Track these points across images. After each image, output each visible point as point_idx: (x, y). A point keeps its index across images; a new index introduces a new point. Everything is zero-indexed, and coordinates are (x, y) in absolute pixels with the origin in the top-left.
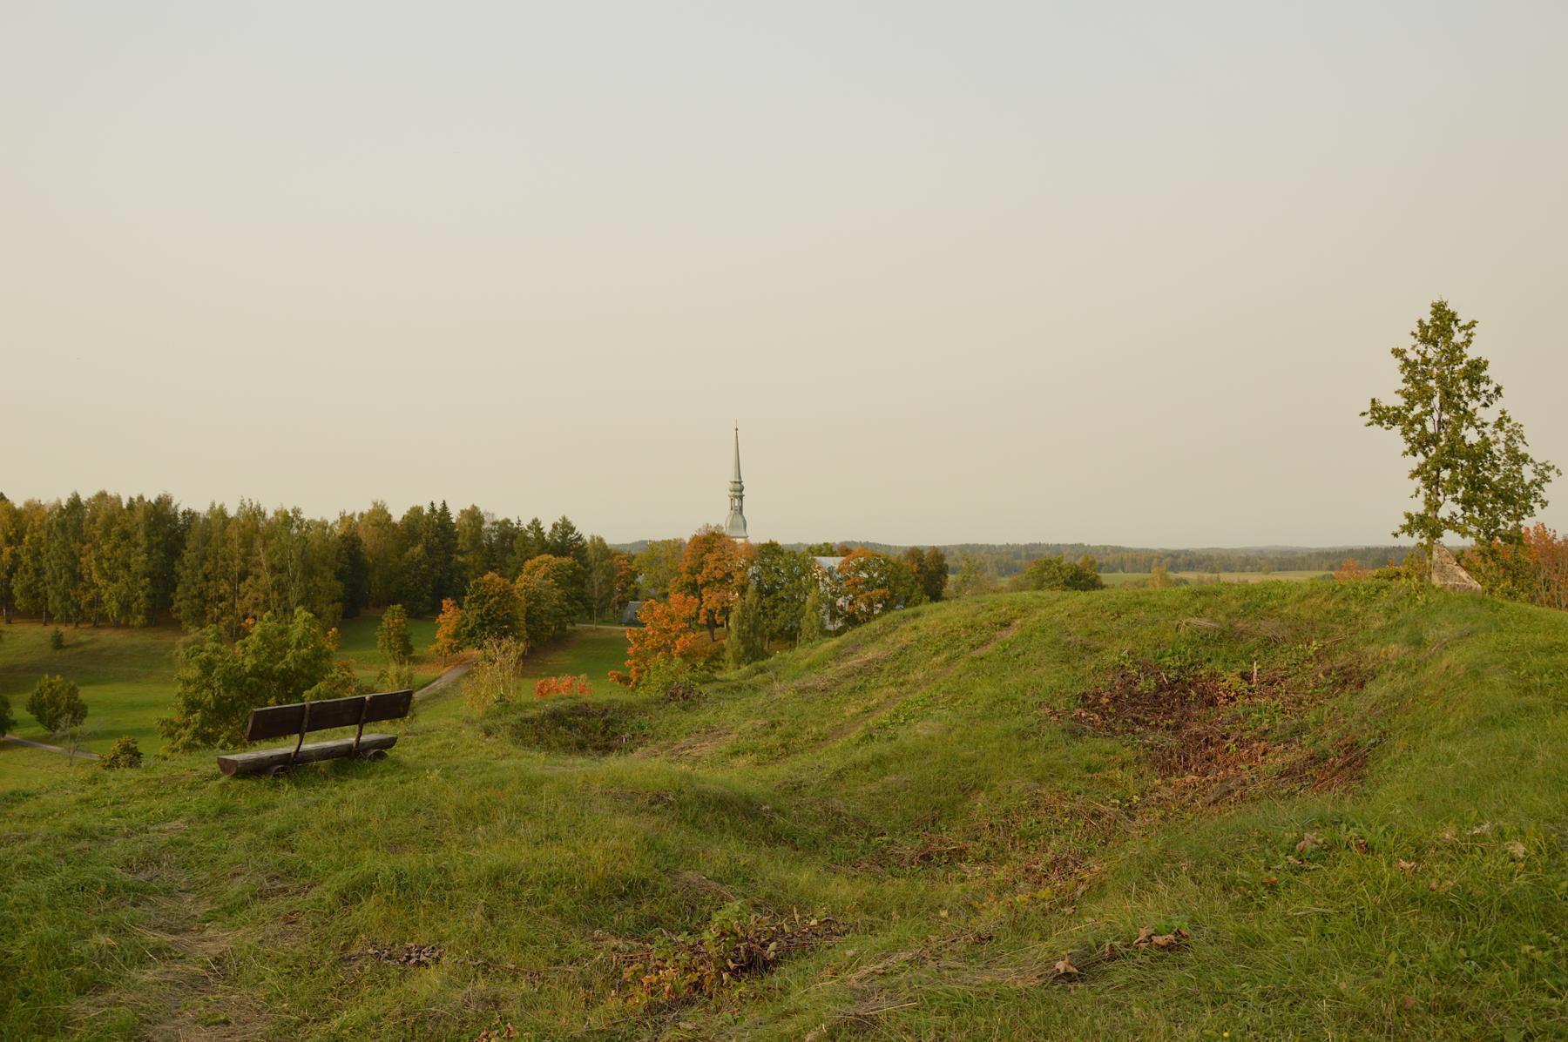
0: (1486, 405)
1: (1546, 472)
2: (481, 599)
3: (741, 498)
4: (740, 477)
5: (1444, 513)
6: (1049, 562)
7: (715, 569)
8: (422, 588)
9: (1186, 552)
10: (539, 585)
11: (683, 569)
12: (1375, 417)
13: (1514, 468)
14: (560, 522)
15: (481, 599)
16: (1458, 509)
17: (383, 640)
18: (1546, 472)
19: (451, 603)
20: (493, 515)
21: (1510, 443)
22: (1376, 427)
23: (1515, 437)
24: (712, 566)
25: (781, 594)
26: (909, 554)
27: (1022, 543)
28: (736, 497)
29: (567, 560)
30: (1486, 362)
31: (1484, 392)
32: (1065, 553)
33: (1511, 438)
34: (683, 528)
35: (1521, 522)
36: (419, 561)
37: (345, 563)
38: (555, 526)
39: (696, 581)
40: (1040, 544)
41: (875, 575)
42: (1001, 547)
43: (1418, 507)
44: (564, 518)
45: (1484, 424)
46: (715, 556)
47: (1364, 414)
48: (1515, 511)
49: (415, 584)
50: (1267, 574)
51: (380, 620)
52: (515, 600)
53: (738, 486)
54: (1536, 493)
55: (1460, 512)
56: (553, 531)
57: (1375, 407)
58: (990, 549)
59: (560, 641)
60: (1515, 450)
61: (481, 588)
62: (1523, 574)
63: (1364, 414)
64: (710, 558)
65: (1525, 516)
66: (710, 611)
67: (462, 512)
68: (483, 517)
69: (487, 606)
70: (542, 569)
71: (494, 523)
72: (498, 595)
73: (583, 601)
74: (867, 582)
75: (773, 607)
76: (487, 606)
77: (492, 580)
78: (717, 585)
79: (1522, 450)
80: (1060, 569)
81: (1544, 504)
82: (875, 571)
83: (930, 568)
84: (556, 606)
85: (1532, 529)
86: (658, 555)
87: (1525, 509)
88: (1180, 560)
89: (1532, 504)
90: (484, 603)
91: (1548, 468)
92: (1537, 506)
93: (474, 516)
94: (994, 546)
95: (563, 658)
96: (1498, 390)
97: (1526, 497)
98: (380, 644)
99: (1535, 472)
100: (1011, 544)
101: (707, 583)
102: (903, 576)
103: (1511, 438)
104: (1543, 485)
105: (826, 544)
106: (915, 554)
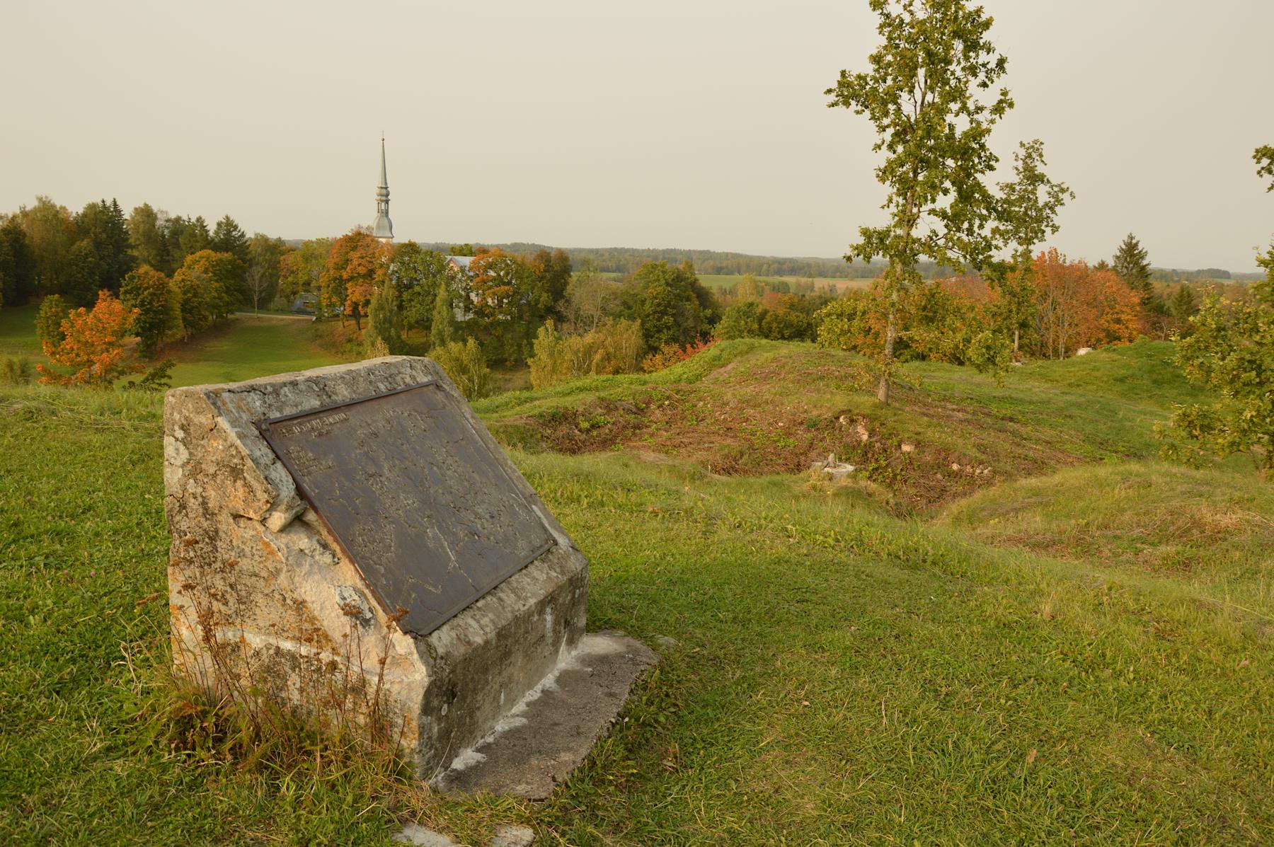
0: (984, 85)
1: (1060, 194)
2: (136, 291)
3: (387, 202)
4: (386, 183)
5: (920, 231)
6: (654, 267)
7: (359, 265)
8: (90, 280)
9: (791, 260)
10: (198, 278)
11: (331, 265)
12: (842, 95)
13: (1030, 188)
14: (224, 221)
15: (136, 291)
16: (940, 226)
17: (42, 328)
18: (1060, 194)
19: (108, 293)
20: (167, 213)
21: (1029, 161)
22: (841, 109)
23: (1034, 155)
24: (355, 262)
25: (417, 289)
26: (538, 256)
27: (661, 248)
28: (382, 201)
29: (227, 256)
30: (991, 17)
31: (984, 65)
32: (694, 258)
33: (1029, 156)
34: (338, 229)
35: (1031, 247)
36: (86, 254)
37: (7, 254)
38: (219, 225)
39: (341, 276)
40: (675, 250)
41: (502, 274)
42: (643, 251)
43: (883, 220)
44: (227, 217)
45: (979, 109)
46: (358, 254)
47: (829, 91)
48: (1027, 235)
49: (83, 276)
50: (852, 280)
51: (38, 309)
52: (169, 292)
53: (384, 192)
54: (1048, 217)
55: (942, 231)
56: (218, 229)
57: (844, 83)
58: (633, 252)
59: (221, 328)
60: (1032, 170)
61: (136, 280)
62: (1028, 302)
63: (829, 91)
64: (354, 256)
65: (1035, 241)
66: (355, 303)
67: (136, 209)
68: (156, 215)
69: (141, 297)
70: (201, 263)
71: (168, 221)
72: (152, 287)
73: (242, 292)
74: (494, 279)
75: (411, 300)
76: (141, 297)
77: (146, 273)
78: (361, 280)
79: (1040, 169)
80: (664, 272)
81: (1055, 229)
82: (502, 270)
83: (555, 268)
84: (214, 298)
85: (1046, 254)
86: (310, 252)
87: (1036, 233)
88: (785, 267)
89: (1043, 228)
90: (139, 295)
91: (1063, 191)
92: (1048, 230)
93: (146, 214)
94: (637, 250)
95: (223, 345)
96: (1001, 63)
97: (1039, 220)
98: (39, 331)
99: (1049, 194)
100: (651, 248)
101: (351, 279)
102: (526, 275)
103: (1029, 156)
104: (1056, 209)
105: (466, 245)
106: (544, 255)
